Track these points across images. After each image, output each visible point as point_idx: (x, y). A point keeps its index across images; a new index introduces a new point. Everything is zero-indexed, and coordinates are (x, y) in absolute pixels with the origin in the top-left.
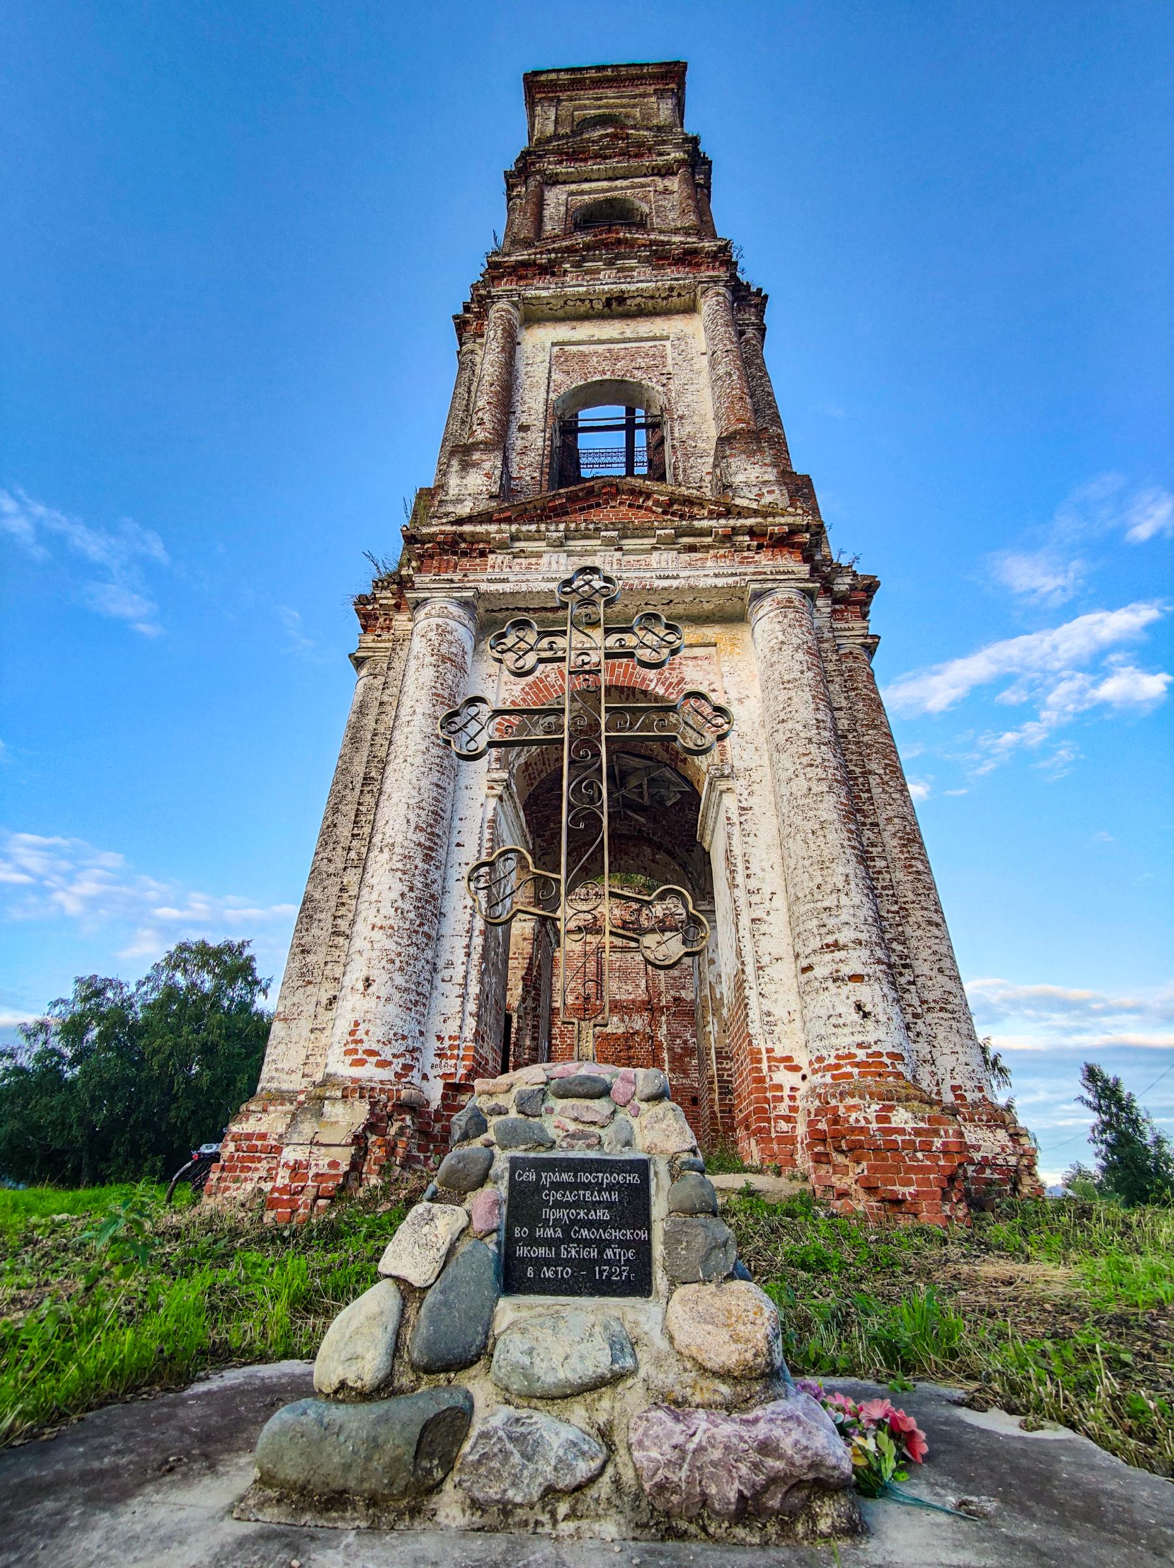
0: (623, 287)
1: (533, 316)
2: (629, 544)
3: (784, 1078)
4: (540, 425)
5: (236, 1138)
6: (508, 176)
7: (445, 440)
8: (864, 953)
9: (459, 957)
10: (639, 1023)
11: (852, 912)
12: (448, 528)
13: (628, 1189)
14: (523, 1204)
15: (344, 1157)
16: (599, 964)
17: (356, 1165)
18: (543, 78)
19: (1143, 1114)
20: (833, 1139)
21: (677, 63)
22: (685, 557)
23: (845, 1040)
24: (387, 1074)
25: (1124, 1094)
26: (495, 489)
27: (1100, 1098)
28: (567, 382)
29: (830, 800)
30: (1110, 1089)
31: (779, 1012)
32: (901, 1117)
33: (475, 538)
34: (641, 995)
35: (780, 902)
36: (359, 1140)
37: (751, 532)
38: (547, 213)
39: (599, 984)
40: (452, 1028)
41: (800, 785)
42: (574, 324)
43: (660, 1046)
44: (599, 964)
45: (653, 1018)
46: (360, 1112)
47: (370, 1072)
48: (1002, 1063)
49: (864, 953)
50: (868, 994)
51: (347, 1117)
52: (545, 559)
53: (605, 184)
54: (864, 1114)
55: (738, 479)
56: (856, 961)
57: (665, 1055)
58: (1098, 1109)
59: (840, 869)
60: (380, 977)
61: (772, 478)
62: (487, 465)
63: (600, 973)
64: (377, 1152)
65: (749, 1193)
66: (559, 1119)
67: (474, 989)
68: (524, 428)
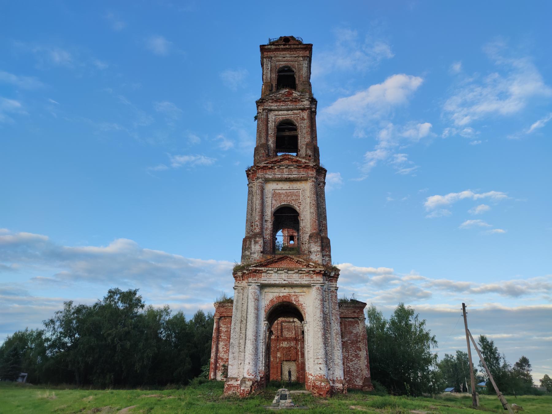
0: (290, 176)
1: (267, 181)
2: (289, 272)
3: (310, 377)
4: (270, 220)
5: (228, 385)
6: (257, 102)
7: (247, 220)
8: (322, 360)
9: (261, 357)
10: (293, 344)
11: (322, 352)
12: (255, 268)
13: (286, 396)
14: (281, 396)
15: (249, 389)
16: (282, 326)
17: (251, 391)
18: (266, 47)
19: (501, 355)
20: (314, 387)
21: (309, 44)
22: (300, 275)
23: (318, 373)
24: (253, 377)
25: (494, 348)
26: (262, 250)
27: (484, 349)
28: (277, 205)
29: (320, 333)
30: (488, 345)
31: (310, 367)
32: (323, 384)
33: (259, 270)
34: (293, 335)
35: (312, 348)
36: (251, 387)
37: (313, 271)
38: (269, 125)
39: (282, 332)
40: (261, 368)
41: (316, 329)
42: (277, 182)
43: (298, 351)
44: (282, 326)
45: (296, 342)
46: (251, 383)
47: (251, 377)
48: (436, 339)
49: (322, 360)
50: (321, 366)
51: (249, 383)
52: (273, 275)
53: (285, 112)
54: (318, 383)
55: (312, 250)
56: (320, 361)
57: (300, 353)
58: (483, 353)
59: (320, 346)
60: (251, 362)
61: (319, 250)
62: (260, 242)
63: (282, 329)
64: (253, 388)
65: (303, 393)
66: (283, 392)
67: (264, 362)
68: (266, 221)
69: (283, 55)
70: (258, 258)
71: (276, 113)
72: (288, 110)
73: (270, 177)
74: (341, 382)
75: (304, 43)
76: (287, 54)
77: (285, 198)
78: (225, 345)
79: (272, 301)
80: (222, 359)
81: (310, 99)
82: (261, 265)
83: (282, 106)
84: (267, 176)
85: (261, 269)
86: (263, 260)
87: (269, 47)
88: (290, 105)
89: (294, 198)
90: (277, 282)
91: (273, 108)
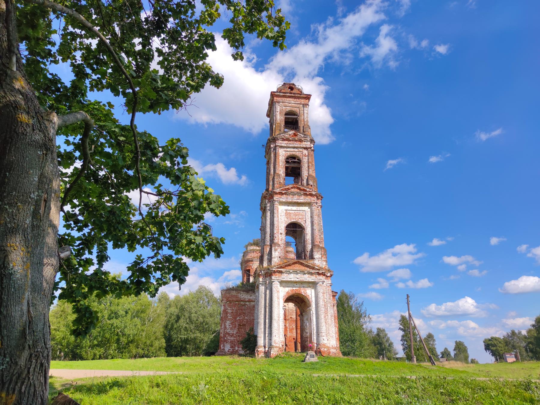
53: (292, 150)
69: (289, 101)
70: (277, 262)
71: (285, 149)
72: (294, 148)
73: (284, 200)
74: (335, 348)
75: (305, 93)
76: (292, 100)
77: (294, 217)
78: (231, 324)
79: (288, 292)
80: (229, 334)
81: (530, 354)
82: (281, 267)
83: (292, 144)
84: (281, 200)
85: (281, 270)
86: (281, 263)
87: (278, 94)
88: (297, 144)
89: (300, 217)
90: (293, 280)
91: (283, 145)
